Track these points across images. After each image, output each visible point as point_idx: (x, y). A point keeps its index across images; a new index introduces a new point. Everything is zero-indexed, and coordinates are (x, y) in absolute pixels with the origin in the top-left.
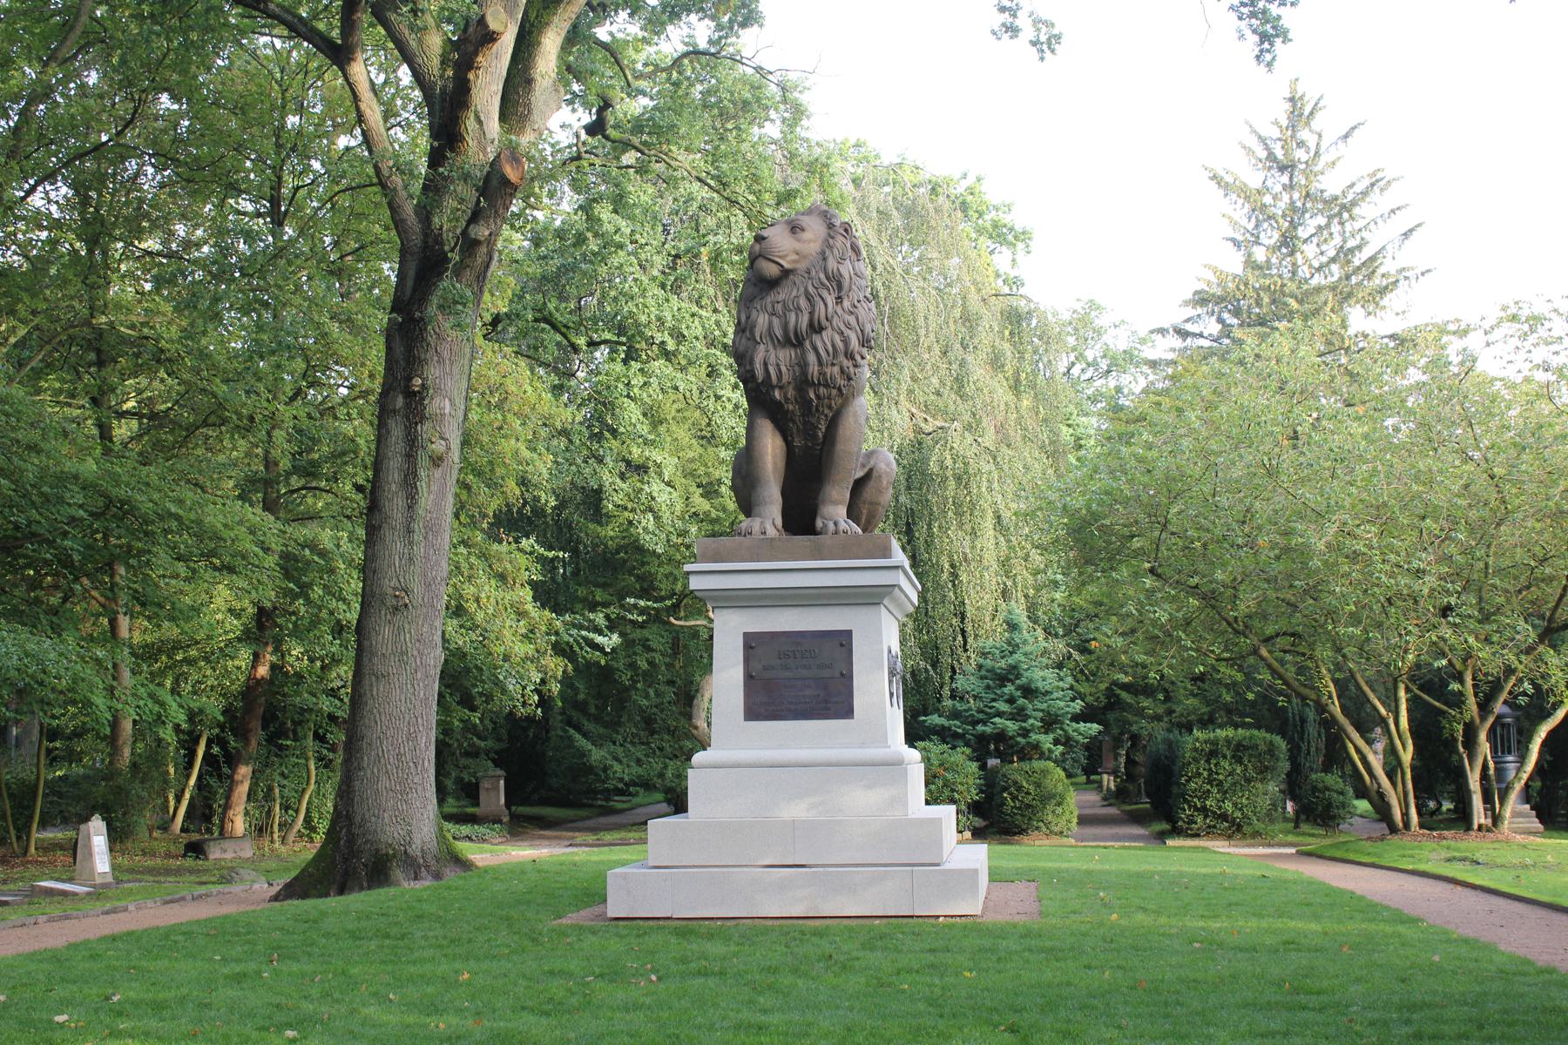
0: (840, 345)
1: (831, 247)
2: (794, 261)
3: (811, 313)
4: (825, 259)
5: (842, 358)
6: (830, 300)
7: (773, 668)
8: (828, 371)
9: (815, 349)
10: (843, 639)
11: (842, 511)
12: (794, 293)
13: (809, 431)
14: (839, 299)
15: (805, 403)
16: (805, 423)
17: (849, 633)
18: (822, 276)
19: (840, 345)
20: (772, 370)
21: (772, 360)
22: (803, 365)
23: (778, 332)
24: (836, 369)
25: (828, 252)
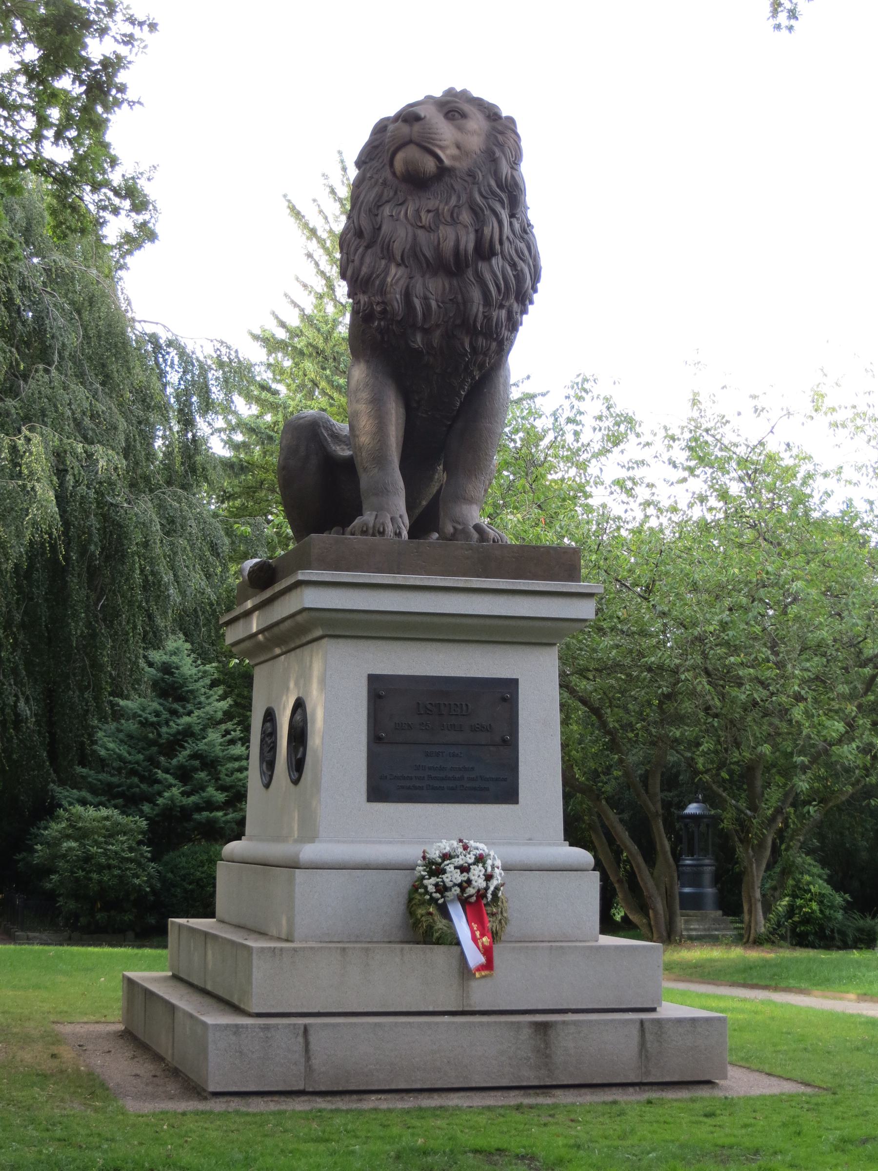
3: (479, 233)
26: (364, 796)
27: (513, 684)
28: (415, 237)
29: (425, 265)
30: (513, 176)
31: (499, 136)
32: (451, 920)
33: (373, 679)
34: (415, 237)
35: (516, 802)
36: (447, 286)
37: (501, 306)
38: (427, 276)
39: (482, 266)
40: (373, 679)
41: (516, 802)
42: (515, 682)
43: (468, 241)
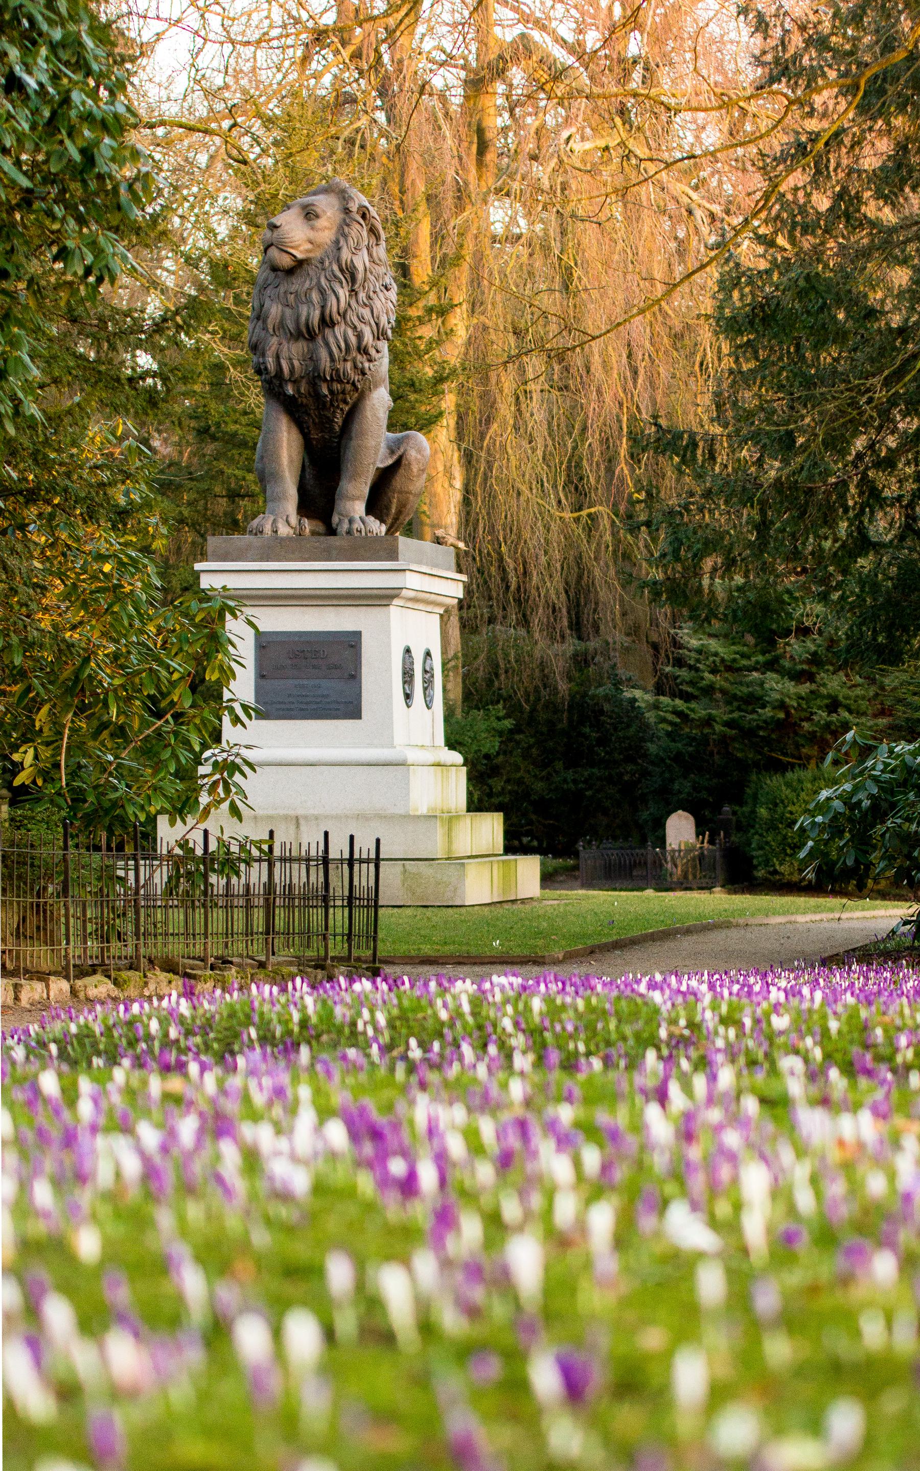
0: (353, 340)
1: (345, 236)
2: (308, 251)
3: (323, 307)
4: (339, 249)
5: (354, 353)
6: (343, 293)
7: (283, 667)
8: (340, 366)
9: (327, 345)
10: (351, 642)
11: (359, 508)
12: (307, 285)
13: (325, 423)
14: (353, 292)
15: (316, 395)
16: (320, 416)
17: (358, 634)
18: (335, 268)
19: (353, 340)
21: (284, 354)
22: (312, 358)
23: (291, 325)
24: (349, 365)
25: (342, 242)
37: (345, 360)
39: (327, 331)
43: (316, 315)
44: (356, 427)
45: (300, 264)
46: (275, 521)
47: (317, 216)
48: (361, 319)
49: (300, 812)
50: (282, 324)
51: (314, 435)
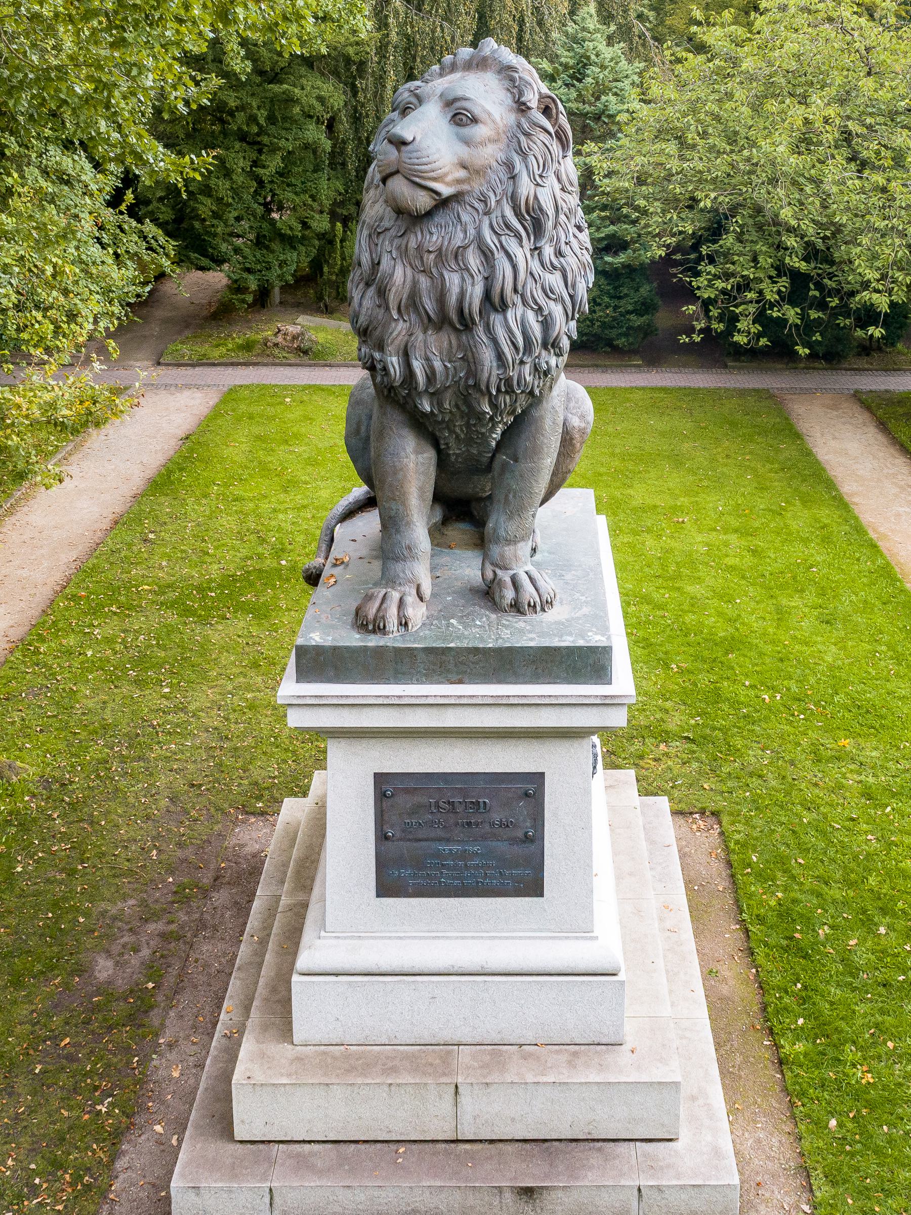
0: (536, 330)
2: (459, 181)
3: (489, 280)
20: (417, 366)
22: (471, 363)
26: (374, 892)
27: (538, 778)
28: (415, 283)
29: (426, 321)
30: (536, 197)
31: (523, 138)
32: (841, 503)
33: (380, 779)
34: (415, 283)
35: (541, 895)
36: (454, 342)
38: (430, 332)
39: (496, 319)
40: (380, 779)
41: (541, 895)
42: (542, 775)
43: (476, 292)
44: (524, 443)
45: (443, 203)
46: (401, 603)
47: (474, 120)
48: (548, 292)
49: (447, 1035)
50: (413, 301)
51: (454, 450)
